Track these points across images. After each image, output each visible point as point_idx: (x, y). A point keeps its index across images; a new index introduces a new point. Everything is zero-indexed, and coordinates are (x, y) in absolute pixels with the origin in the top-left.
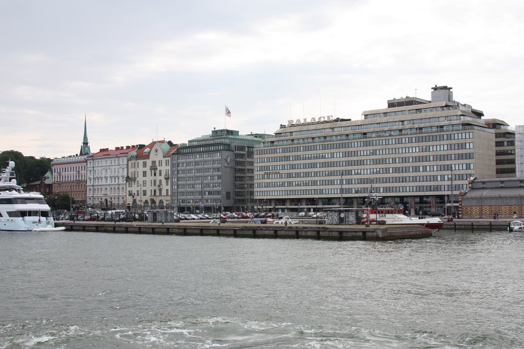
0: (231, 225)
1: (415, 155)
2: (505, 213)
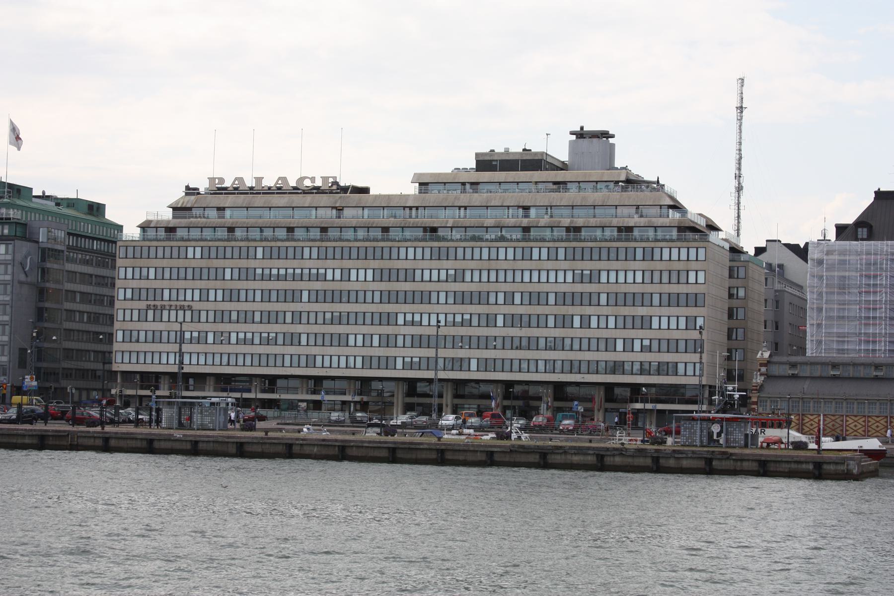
0: (289, 435)
1: (562, 288)
2: (855, 431)
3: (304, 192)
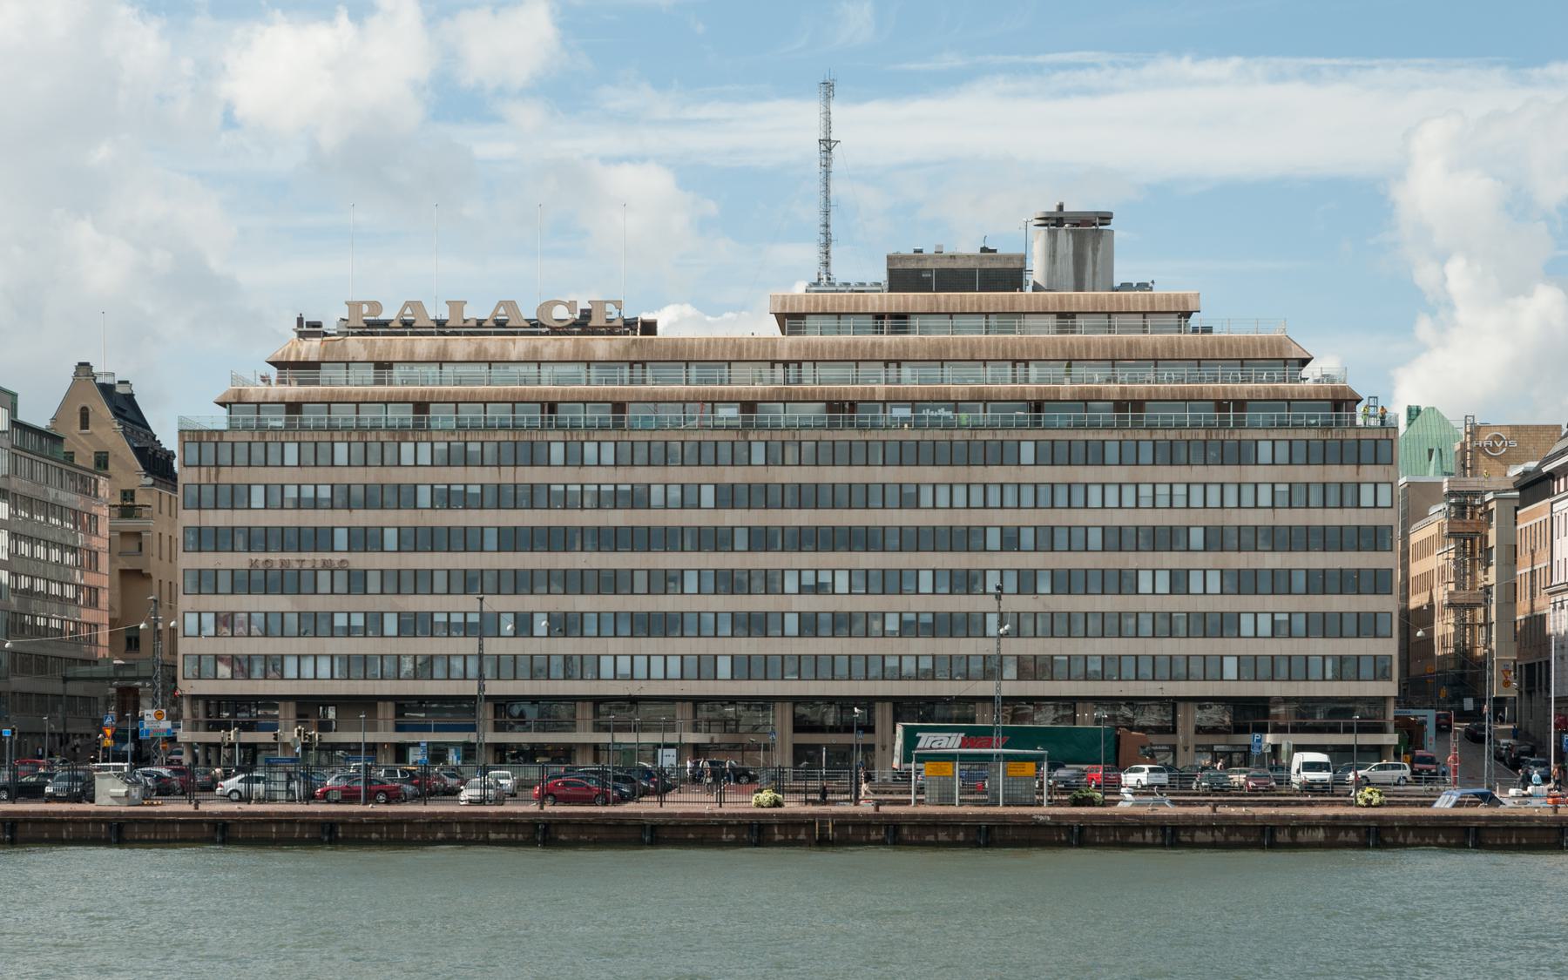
3: (554, 331)
